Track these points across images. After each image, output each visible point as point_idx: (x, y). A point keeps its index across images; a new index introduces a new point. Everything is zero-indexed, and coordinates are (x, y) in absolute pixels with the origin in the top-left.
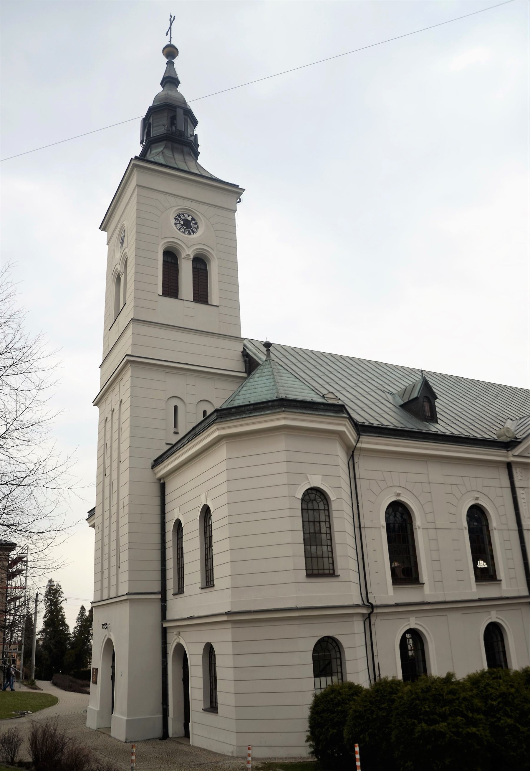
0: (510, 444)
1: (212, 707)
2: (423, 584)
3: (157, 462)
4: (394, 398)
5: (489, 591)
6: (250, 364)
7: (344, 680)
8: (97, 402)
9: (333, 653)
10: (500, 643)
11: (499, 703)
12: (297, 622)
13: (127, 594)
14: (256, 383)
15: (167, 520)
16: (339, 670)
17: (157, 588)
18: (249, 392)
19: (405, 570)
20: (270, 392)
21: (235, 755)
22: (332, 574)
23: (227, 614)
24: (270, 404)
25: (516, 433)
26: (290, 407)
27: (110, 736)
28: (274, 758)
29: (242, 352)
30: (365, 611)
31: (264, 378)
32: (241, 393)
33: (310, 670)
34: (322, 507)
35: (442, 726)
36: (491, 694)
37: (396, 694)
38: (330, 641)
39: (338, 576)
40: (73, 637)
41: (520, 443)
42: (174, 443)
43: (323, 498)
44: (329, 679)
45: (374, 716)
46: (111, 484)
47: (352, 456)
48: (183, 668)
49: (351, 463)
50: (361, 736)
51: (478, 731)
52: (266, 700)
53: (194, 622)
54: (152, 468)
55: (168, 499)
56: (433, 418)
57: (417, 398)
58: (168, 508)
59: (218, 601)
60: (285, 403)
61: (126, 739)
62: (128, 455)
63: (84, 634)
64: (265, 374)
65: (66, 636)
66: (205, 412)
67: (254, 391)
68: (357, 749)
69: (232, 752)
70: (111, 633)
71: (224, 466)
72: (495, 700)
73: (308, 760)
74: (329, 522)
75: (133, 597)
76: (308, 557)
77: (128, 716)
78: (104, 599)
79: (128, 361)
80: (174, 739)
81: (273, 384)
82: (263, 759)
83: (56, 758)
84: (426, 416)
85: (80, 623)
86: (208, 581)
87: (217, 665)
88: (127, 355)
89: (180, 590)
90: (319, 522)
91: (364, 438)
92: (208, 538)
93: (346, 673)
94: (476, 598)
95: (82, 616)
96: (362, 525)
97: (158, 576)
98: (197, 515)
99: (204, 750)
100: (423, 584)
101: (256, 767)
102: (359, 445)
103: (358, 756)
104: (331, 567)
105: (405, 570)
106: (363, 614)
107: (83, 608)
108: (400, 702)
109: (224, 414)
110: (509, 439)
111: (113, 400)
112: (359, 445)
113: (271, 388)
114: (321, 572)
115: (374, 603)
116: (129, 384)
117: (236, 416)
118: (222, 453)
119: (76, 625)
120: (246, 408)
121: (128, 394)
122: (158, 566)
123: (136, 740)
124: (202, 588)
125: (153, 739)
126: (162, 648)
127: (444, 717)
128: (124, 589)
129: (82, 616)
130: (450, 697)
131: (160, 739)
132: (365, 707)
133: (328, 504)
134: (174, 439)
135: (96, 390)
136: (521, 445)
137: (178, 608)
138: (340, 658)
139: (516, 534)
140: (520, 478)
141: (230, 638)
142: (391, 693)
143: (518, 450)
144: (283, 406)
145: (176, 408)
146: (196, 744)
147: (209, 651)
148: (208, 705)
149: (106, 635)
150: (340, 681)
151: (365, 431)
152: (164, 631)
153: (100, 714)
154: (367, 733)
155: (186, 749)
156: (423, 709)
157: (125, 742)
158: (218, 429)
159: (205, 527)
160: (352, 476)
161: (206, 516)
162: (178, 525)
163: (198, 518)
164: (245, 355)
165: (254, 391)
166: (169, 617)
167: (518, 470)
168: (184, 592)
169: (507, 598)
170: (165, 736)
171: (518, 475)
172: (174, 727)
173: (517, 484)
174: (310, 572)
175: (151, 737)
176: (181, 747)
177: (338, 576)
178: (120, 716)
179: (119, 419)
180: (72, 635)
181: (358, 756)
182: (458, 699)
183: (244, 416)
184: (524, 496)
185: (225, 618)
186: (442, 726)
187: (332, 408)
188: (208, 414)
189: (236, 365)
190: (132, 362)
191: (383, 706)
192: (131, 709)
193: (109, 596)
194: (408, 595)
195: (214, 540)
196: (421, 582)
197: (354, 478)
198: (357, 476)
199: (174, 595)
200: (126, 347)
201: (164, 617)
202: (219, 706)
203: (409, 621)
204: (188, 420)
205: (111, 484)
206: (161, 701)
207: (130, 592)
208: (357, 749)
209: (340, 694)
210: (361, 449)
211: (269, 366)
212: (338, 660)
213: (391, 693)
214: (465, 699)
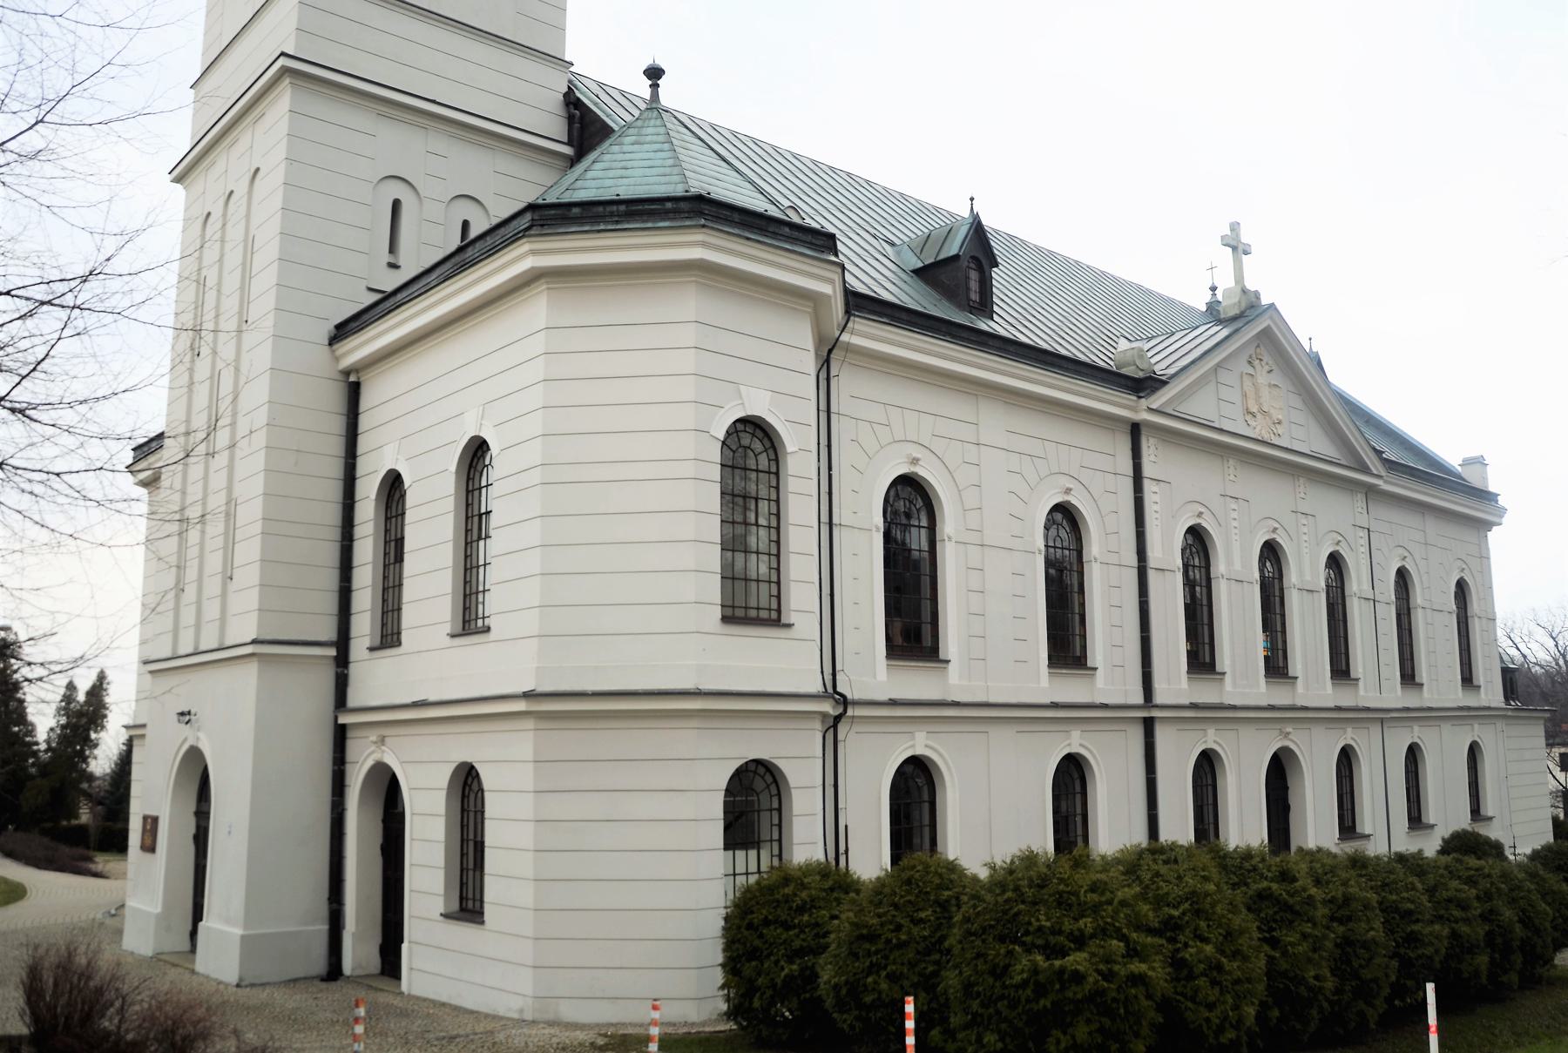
0: (1143, 385)
1: (468, 905)
2: (948, 662)
3: (343, 331)
4: (898, 253)
5: (1071, 689)
6: (585, 128)
7: (784, 856)
8: (182, 174)
9: (764, 798)
10: (1078, 797)
11: (1184, 914)
12: (694, 723)
13: (254, 642)
14: (628, 156)
15: (360, 471)
16: (776, 836)
17: (328, 632)
18: (611, 173)
19: (913, 628)
20: (663, 179)
21: (528, 1016)
22: (774, 619)
23: (528, 695)
24: (669, 205)
25: (1153, 361)
26: (717, 218)
27: (193, 972)
28: (624, 1024)
29: (565, 95)
30: (828, 707)
31: (646, 147)
32: (590, 174)
33: (715, 832)
34: (763, 462)
35: (1077, 960)
36: (1168, 893)
37: (948, 889)
38: (761, 770)
39: (789, 626)
40: (46, 751)
41: (1165, 383)
42: (389, 288)
43: (768, 444)
44: (753, 853)
45: (903, 937)
46: (215, 378)
47: (827, 361)
48: (384, 821)
49: (823, 375)
50: (870, 980)
51: (1153, 969)
52: (612, 891)
53: (424, 714)
54: (330, 344)
55: (364, 422)
56: (985, 306)
57: (956, 258)
58: (363, 444)
59: (503, 663)
60: (706, 208)
61: (241, 979)
62: (272, 305)
63: (72, 744)
64: (649, 138)
65: (28, 749)
66: (466, 225)
67: (623, 173)
68: (910, 1008)
69: (521, 1011)
70: (201, 735)
71: (538, 344)
72: (1175, 907)
73: (707, 1029)
74: (778, 501)
75: (269, 649)
76: (732, 578)
77: (246, 927)
78: (182, 652)
79: (285, 71)
80: (355, 980)
81: (671, 162)
82: (603, 1025)
83: (732, 1026)
84: (969, 299)
85: (63, 720)
86: (470, 620)
87: (487, 815)
88: (283, 54)
89: (389, 637)
90: (757, 499)
91: (858, 324)
92: (476, 519)
93: (792, 844)
94: (1047, 701)
95: (69, 703)
96: (835, 520)
97: (330, 604)
98: (450, 460)
99: (443, 1004)
100: (948, 662)
101: (592, 1044)
102: (845, 337)
103: (910, 1024)
104: (774, 606)
105: (913, 628)
106: (824, 715)
107: (71, 687)
108: (975, 907)
109: (546, 217)
110: (1141, 375)
111: (230, 166)
112: (845, 337)
113: (668, 170)
114: (753, 613)
115: (849, 696)
116: (283, 127)
117: (582, 224)
118: (537, 310)
119: (53, 723)
120: (609, 209)
121: (281, 152)
122: (331, 579)
123: (264, 980)
124: (453, 636)
125: (305, 978)
126: (334, 773)
127: (1080, 941)
128: (244, 628)
129: (69, 703)
130: (1094, 897)
131: (323, 980)
132: (879, 916)
133: (777, 460)
134: (391, 281)
135: (180, 140)
136: (1167, 387)
137: (378, 679)
138: (780, 810)
139: (1133, 575)
140: (1152, 458)
141: (529, 755)
142: (940, 887)
143: (1159, 399)
144: (701, 214)
145: (396, 205)
146: (416, 992)
147: (467, 783)
148: (455, 906)
149: (185, 740)
150: (776, 862)
151: (859, 308)
152: (341, 735)
153: (164, 919)
154: (884, 973)
155: (397, 1002)
156: (1036, 924)
157: (238, 986)
158: (534, 252)
159: (468, 492)
160: (823, 406)
161: (390, 497)
162: (393, 485)
163: (453, 468)
164: (572, 102)
165: (623, 173)
166: (353, 700)
167: (1152, 440)
168: (399, 644)
169: (1105, 706)
170: (334, 972)
171: (1151, 450)
172: (358, 951)
173: (1147, 470)
174: (729, 612)
175: (300, 972)
176: (383, 998)
177: (789, 626)
178: (224, 926)
179: (248, 216)
180: (43, 747)
181: (910, 1024)
182: (1110, 902)
183: (602, 227)
184: (1156, 498)
185: (521, 706)
186: (1077, 960)
187: (809, 238)
188: (474, 232)
189: (551, 125)
190: (294, 72)
191: (923, 915)
192: (252, 911)
193: (196, 647)
194: (915, 682)
195: (408, 546)
196: (942, 656)
197: (826, 412)
198: (833, 408)
199: (372, 649)
200: (279, 33)
201: (341, 701)
202: (487, 909)
203: (913, 738)
204: (427, 241)
205: (215, 378)
206: (326, 895)
207: (262, 637)
208: (910, 1008)
209: (803, 886)
210: (849, 348)
211: (659, 122)
212: (775, 814)
213: (940, 887)
214: (1123, 903)
